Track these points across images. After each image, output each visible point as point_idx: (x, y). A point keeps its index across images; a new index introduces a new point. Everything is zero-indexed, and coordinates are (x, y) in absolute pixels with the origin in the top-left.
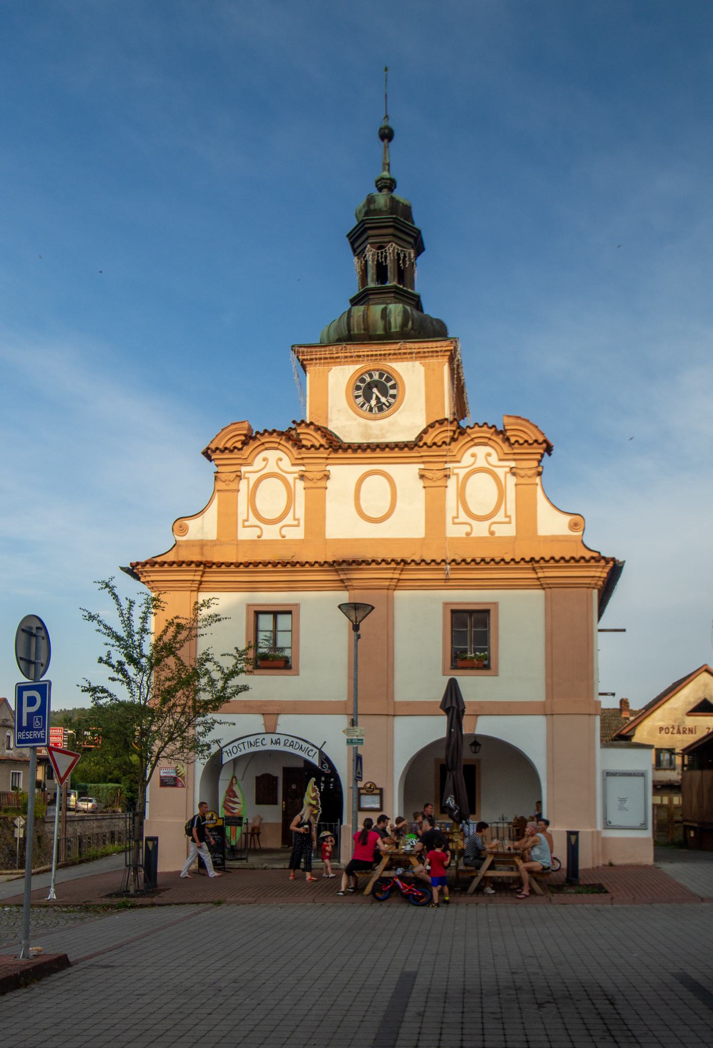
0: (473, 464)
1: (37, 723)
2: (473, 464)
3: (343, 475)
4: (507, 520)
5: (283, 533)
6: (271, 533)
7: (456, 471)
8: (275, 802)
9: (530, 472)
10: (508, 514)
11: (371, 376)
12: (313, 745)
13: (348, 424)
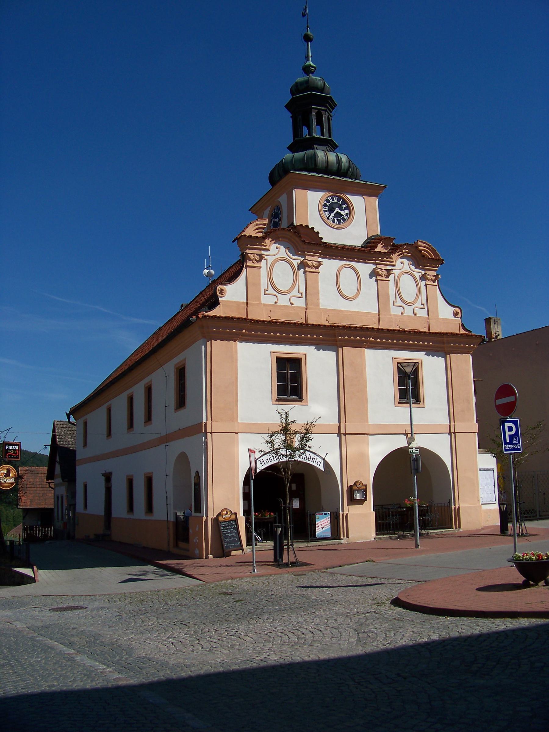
0: (403, 267)
1: (515, 441)
2: (403, 267)
3: (330, 266)
4: (300, 295)
5: (292, 301)
6: (283, 300)
11: (333, 199)
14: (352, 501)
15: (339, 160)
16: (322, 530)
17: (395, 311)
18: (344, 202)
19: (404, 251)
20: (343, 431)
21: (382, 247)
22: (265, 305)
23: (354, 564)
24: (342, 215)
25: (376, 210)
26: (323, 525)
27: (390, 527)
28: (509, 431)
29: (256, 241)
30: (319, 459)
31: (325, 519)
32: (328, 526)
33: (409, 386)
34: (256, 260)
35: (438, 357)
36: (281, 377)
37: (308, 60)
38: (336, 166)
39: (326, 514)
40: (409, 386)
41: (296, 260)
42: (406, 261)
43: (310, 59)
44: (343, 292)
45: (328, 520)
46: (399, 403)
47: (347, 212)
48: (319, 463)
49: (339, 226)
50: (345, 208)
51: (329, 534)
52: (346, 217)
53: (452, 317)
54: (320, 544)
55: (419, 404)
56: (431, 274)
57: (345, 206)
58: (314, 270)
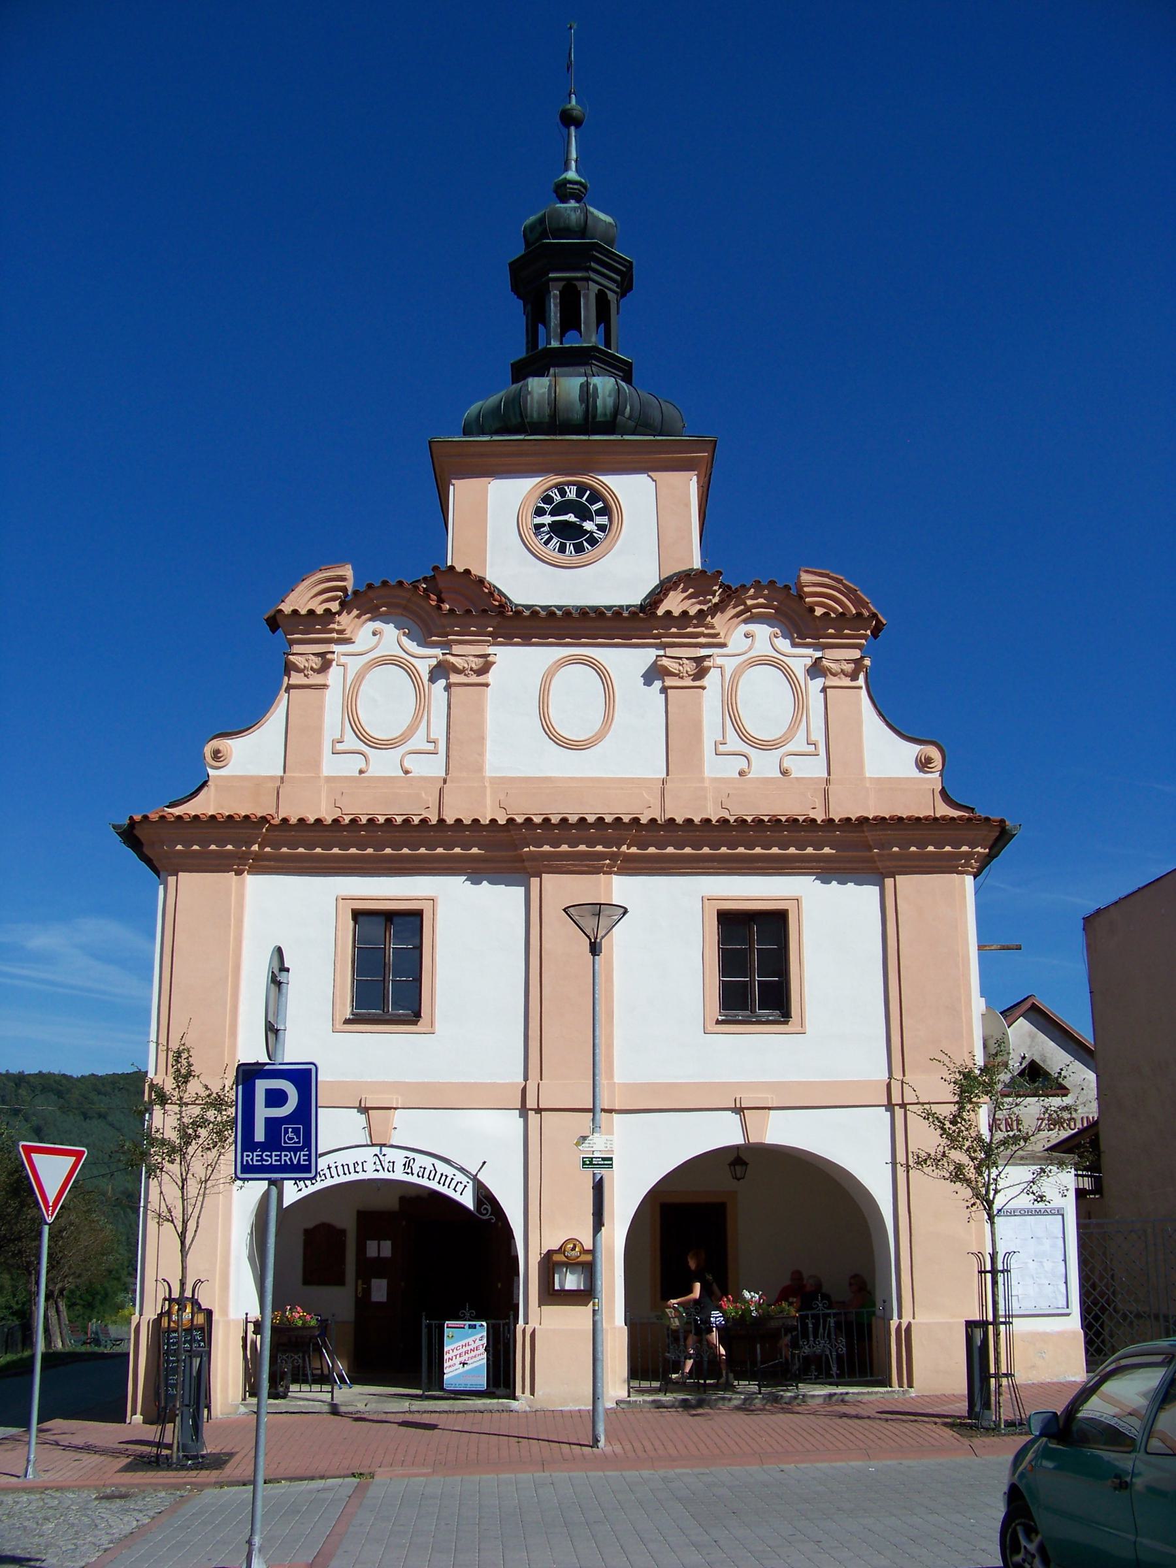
0: (750, 649)
1: (289, 1136)
2: (750, 649)
3: (517, 665)
4: (431, 747)
5: (407, 765)
6: (383, 764)
7: (719, 661)
8: (340, 1281)
9: (849, 667)
10: (813, 738)
11: (563, 493)
12: (462, 1170)
13: (522, 574)
14: (552, 1295)
15: (587, 394)
16: (461, 1369)
17: (718, 768)
18: (595, 497)
19: (749, 602)
20: (531, 1103)
21: (689, 597)
22: (329, 779)
23: (312, 1478)
24: (586, 532)
25: (688, 505)
26: (464, 1352)
27: (829, 1368)
28: (269, 1104)
29: (314, 623)
30: (460, 1177)
31: (470, 1340)
32: (480, 1360)
33: (755, 972)
34: (312, 669)
35: (842, 882)
36: (731, 962)
37: (567, 168)
38: (578, 409)
39: (474, 1327)
40: (755, 972)
41: (425, 658)
42: (763, 631)
43: (573, 163)
44: (557, 728)
45: (478, 1343)
46: (718, 1022)
47: (603, 520)
48: (460, 1188)
49: (583, 557)
50: (599, 513)
51: (481, 1382)
52: (599, 535)
53: (915, 773)
54: (447, 1408)
55: (786, 1023)
56: (841, 656)
57: (600, 505)
58: (474, 679)
